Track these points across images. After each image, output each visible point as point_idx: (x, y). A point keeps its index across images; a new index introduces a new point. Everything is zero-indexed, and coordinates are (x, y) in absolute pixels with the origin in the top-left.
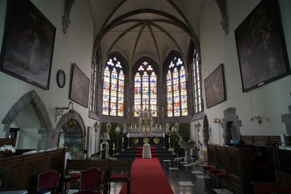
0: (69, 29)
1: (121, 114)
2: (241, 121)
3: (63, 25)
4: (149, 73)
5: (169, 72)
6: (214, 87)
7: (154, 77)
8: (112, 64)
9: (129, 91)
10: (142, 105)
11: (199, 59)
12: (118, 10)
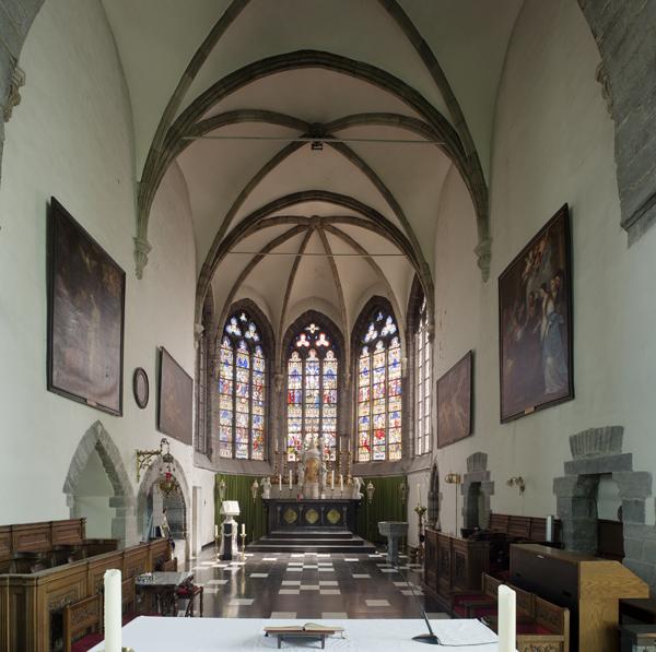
0: (147, 267)
1: (258, 455)
2: (493, 483)
3: (137, 259)
4: (321, 353)
5: (365, 350)
6: (454, 401)
7: (331, 365)
8: (238, 333)
9: (275, 397)
10: (303, 433)
11: (431, 328)
12: (249, 197)
